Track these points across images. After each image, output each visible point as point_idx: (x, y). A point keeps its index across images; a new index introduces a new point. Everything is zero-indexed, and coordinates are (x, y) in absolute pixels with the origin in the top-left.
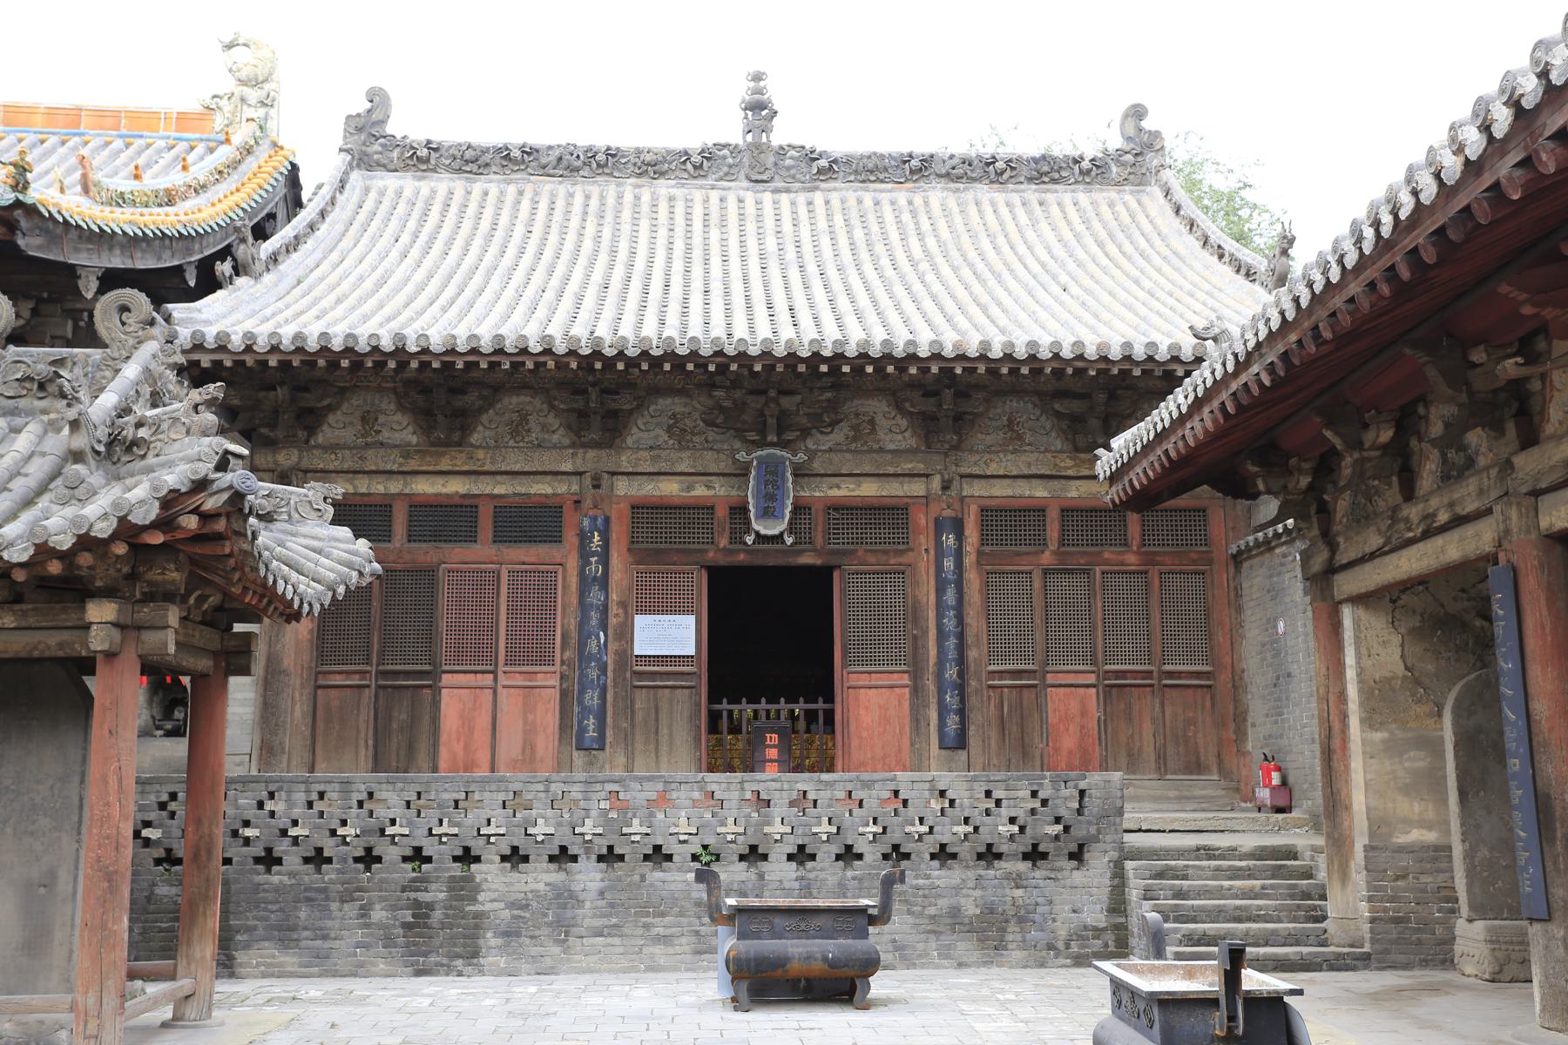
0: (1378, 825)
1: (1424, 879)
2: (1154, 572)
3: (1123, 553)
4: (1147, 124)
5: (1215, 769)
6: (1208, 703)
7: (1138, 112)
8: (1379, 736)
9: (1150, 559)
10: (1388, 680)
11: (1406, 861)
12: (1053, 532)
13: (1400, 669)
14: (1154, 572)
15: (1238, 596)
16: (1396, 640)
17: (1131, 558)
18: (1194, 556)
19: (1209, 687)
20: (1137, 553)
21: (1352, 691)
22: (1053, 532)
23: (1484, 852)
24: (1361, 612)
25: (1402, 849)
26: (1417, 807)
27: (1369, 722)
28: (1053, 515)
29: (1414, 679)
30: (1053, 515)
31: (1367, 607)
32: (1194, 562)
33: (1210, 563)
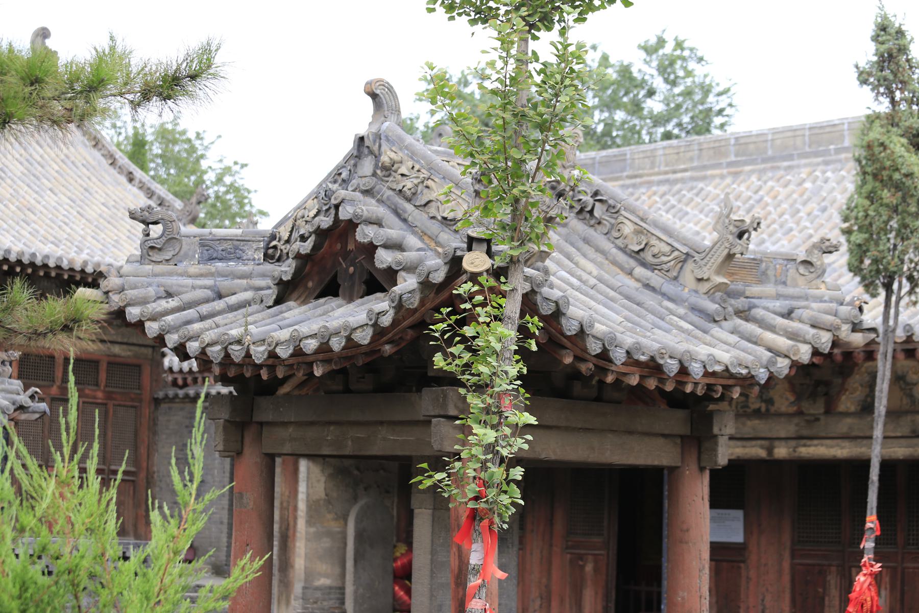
0: (309, 575)
1: (325, 603)
2: (111, 404)
3: (95, 391)
4: (50, 43)
5: (132, 533)
6: (131, 492)
7: (44, 33)
8: (312, 530)
9: (109, 396)
10: (318, 501)
11: (318, 594)
12: (103, 376)
13: (323, 495)
14: (111, 404)
15: (155, 424)
16: (323, 479)
17: (100, 395)
18: (133, 396)
19: (133, 481)
20: (104, 391)
21: (302, 506)
22: (103, 376)
23: (361, 591)
24: (311, 464)
25: (317, 589)
26: (324, 567)
27: (309, 522)
28: (103, 367)
29: (328, 501)
30: (103, 367)
31: (314, 461)
32: (132, 400)
33: (141, 401)
